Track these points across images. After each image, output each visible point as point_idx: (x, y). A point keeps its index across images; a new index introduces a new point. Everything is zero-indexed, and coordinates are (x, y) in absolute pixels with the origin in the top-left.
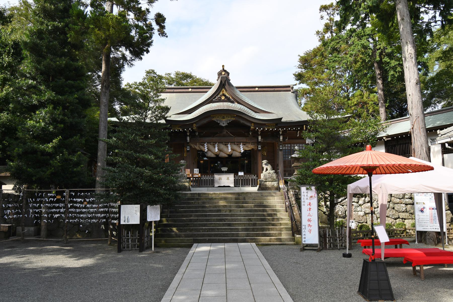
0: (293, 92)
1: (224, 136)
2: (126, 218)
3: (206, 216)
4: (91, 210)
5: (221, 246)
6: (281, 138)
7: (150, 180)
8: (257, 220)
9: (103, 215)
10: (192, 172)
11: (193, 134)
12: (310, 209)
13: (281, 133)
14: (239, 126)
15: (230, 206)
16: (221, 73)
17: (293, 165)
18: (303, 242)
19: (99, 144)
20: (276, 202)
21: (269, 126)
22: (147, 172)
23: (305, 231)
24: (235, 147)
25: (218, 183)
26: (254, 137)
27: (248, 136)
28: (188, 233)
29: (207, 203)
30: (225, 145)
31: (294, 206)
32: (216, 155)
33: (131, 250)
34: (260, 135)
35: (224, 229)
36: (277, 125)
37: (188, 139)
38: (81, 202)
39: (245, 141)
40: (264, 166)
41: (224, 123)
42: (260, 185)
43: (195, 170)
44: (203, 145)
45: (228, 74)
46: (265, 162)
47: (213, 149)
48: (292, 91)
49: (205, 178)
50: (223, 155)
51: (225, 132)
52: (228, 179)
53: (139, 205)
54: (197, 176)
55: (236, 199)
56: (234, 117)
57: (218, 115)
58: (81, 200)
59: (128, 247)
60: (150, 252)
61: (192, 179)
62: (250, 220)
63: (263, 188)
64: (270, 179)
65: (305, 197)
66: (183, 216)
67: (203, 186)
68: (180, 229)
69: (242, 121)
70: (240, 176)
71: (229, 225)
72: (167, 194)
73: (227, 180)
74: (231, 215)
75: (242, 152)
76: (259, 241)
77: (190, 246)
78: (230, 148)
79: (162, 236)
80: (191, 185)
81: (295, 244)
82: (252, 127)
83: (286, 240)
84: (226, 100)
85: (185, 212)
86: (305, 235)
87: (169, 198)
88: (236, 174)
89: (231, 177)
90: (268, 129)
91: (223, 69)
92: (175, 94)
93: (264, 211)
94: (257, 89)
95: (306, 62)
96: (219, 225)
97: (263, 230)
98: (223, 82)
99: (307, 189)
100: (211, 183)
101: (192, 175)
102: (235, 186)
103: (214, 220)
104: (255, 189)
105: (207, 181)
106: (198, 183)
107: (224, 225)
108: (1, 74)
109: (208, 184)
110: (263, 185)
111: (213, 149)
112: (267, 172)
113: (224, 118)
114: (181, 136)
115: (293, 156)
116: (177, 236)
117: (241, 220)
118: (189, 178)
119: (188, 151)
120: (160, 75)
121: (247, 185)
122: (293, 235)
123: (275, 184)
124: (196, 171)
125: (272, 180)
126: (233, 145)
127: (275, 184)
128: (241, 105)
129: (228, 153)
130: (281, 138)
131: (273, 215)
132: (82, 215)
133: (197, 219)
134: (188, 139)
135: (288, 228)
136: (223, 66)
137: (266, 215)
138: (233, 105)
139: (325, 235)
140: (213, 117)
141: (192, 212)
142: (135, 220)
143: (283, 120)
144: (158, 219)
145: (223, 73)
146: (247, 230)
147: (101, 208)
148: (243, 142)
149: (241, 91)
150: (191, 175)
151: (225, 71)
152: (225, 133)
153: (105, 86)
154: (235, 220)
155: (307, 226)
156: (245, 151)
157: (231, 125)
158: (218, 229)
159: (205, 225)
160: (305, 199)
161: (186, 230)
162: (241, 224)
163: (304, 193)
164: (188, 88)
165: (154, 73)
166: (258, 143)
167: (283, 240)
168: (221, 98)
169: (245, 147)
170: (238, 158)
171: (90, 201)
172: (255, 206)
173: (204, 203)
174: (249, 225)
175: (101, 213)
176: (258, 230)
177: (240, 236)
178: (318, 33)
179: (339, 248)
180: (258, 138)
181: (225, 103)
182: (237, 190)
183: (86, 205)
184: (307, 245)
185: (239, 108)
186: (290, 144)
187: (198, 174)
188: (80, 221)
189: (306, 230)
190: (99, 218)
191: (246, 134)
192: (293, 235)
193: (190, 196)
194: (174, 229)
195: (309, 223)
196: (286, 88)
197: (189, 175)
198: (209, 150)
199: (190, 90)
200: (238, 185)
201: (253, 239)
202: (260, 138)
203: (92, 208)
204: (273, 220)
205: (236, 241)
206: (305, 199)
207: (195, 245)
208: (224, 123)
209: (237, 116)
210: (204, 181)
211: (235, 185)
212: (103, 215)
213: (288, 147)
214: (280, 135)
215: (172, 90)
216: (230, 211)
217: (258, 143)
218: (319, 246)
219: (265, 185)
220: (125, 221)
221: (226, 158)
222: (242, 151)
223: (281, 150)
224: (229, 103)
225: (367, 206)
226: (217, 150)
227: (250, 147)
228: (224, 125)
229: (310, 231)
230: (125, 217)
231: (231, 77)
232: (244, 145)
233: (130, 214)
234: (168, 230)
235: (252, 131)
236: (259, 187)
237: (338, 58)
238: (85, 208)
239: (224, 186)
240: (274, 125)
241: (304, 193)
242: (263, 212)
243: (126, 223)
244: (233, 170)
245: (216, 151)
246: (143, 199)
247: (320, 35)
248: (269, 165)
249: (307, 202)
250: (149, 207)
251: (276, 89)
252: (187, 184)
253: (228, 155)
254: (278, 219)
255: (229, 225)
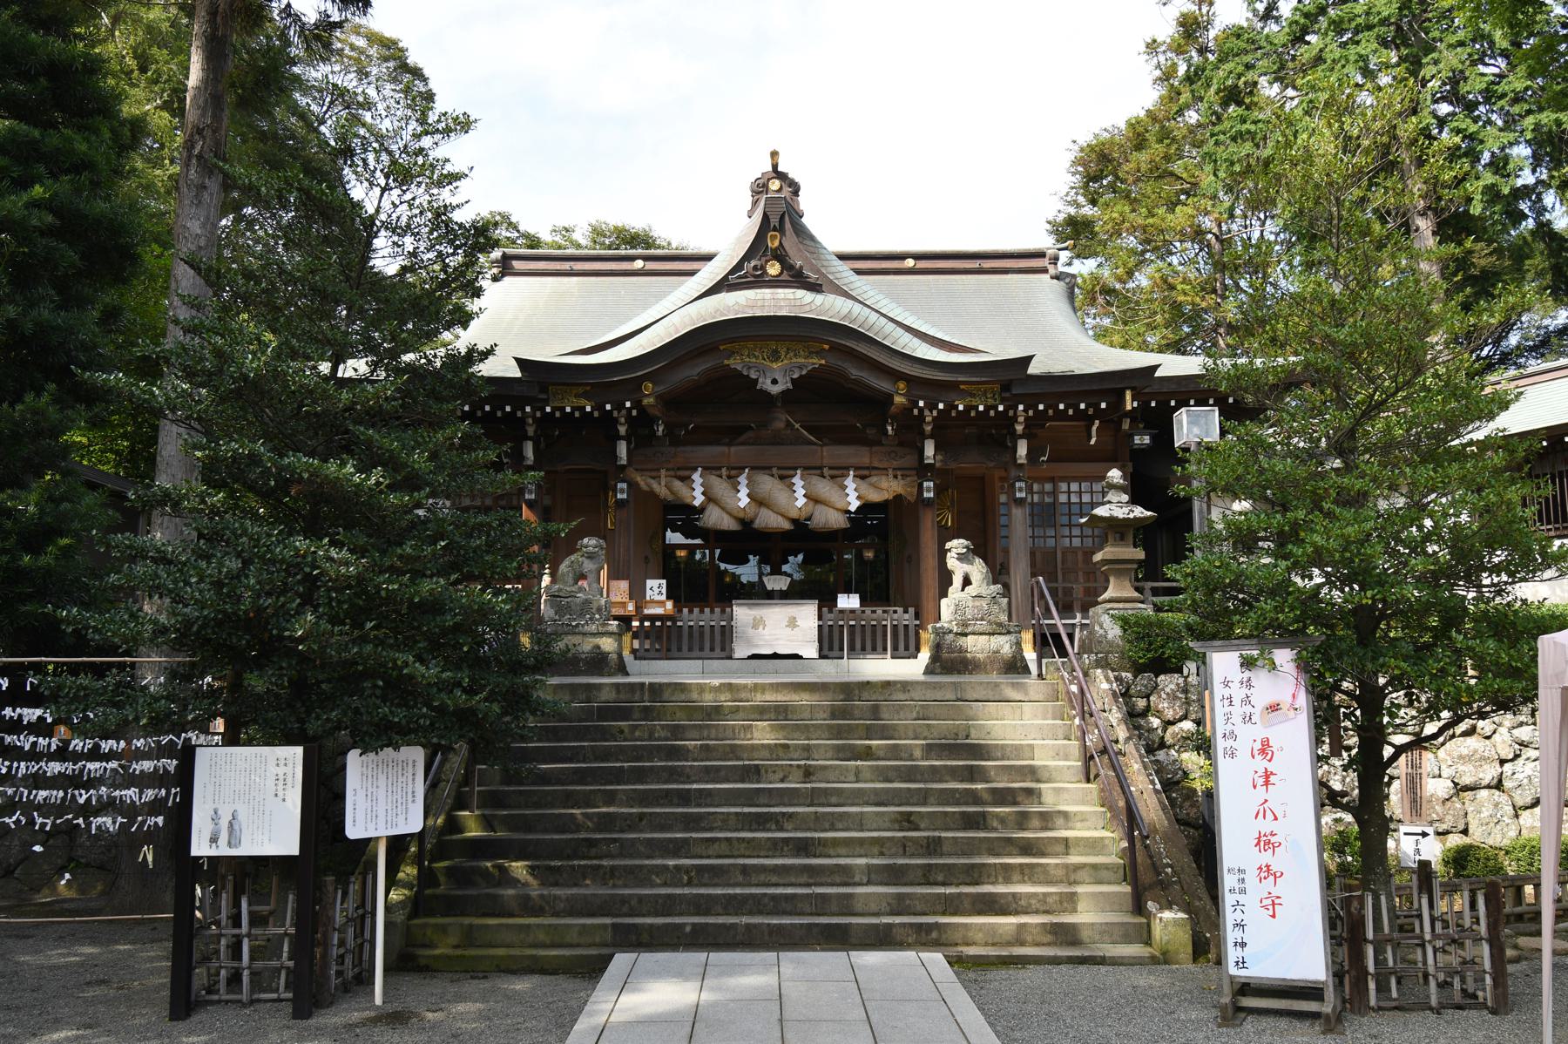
0: (1057, 277)
1: (777, 440)
2: (224, 824)
3: (685, 798)
4: (92, 766)
5: (751, 977)
6: (1022, 450)
7: (360, 604)
8: (946, 822)
9: (150, 794)
10: (637, 593)
11: (641, 425)
12: (1267, 775)
13: (1019, 428)
15: (807, 748)
16: (765, 186)
17: (1098, 557)
18: (1233, 971)
19: (163, 438)
20: (1030, 726)
21: (973, 395)
22: (337, 559)
23: (1242, 905)
24: (824, 488)
25: (749, 642)
26: (901, 444)
27: (879, 443)
28: (590, 889)
29: (695, 734)
30: (782, 478)
31: (1120, 753)
32: (742, 521)
33: (252, 1002)
34: (931, 437)
35: (776, 869)
36: (1006, 387)
37: (622, 449)
38: (40, 728)
39: (866, 461)
40: (952, 562)
41: (775, 377)
42: (937, 648)
43: (650, 583)
44: (686, 480)
45: (795, 188)
46: (957, 545)
47: (732, 498)
48: (1052, 271)
49: (694, 618)
50: (770, 520)
51: (780, 420)
52: (792, 623)
53: (299, 750)
54: (659, 611)
55: (835, 713)
56: (820, 353)
57: (750, 345)
58: (39, 712)
59: (235, 979)
60: (356, 1016)
61: (636, 624)
62: (908, 821)
63: (948, 662)
64: (982, 626)
65: (1238, 711)
66: (570, 800)
67: (696, 653)
68: (550, 868)
69: (855, 372)
70: (842, 611)
71: (803, 847)
72: (459, 684)
73: (783, 628)
74: (814, 797)
75: (853, 508)
76: (957, 937)
77: (593, 969)
78: (800, 492)
79: (452, 906)
80: (634, 651)
81: (1154, 960)
82: (898, 399)
83: (1107, 931)
84: (785, 277)
85: (582, 776)
86: (1240, 925)
87: (473, 712)
88: (826, 601)
89: (807, 615)
90: (968, 409)
91: (775, 167)
93: (972, 774)
94: (910, 263)
95: (1099, 166)
96: (753, 847)
97: (975, 875)
98: (774, 221)
99: (1248, 663)
100: (720, 643)
101: (638, 608)
102: (822, 657)
103: (726, 823)
104: (913, 668)
105: (702, 634)
106: (664, 639)
107: (776, 847)
109: (707, 645)
110: (951, 650)
111: (732, 498)
112: (966, 592)
113: (775, 356)
114: (576, 427)
115: (1101, 511)
116: (528, 907)
117: (860, 823)
118: (625, 620)
119: (621, 504)
120: (532, 231)
121: (874, 649)
122: (1139, 908)
123: (1004, 645)
124: (656, 588)
125: (988, 628)
126: (815, 480)
127: (1004, 645)
128: (850, 303)
129: (794, 514)
130: (1022, 450)
131: (1020, 793)
132: (43, 794)
133: (641, 816)
134: (622, 449)
135: (1106, 867)
136: (774, 154)
137: (986, 796)
138: (819, 299)
139: (1357, 925)
140: (731, 354)
141: (618, 776)
142: (276, 832)
143: (1033, 369)
144: (413, 822)
145: (775, 185)
146: (894, 875)
147: (140, 755)
148: (856, 469)
150: (631, 607)
151: (782, 176)
152: (779, 425)
153: (200, 157)
154: (833, 822)
155: (1251, 877)
156: (866, 507)
157: (806, 390)
158: (745, 869)
159: (678, 848)
160: (1237, 719)
161: (577, 877)
162: (861, 841)
163: (1226, 684)
164: (632, 259)
165: (510, 224)
166: (923, 470)
167: (1085, 935)
168: (763, 268)
169: (864, 485)
170: (832, 535)
171: (86, 719)
172: (929, 750)
173: (677, 732)
174: (904, 847)
175: (142, 781)
176: (951, 875)
177: (859, 907)
178: (1152, 47)
179: (1434, 1002)
180: (921, 451)
182: (831, 671)
183: (66, 743)
184: (1246, 988)
185: (845, 311)
186: (1052, 480)
187: (662, 603)
188: (32, 822)
189: (1251, 900)
190: (131, 811)
191: (871, 432)
192: (1139, 908)
193: (613, 695)
194: (519, 868)
195: (1266, 858)
196: (1026, 261)
197: (624, 605)
198: (710, 498)
199: (639, 264)
200: (836, 653)
201: (929, 928)
202: (929, 450)
203: (95, 754)
204: (1022, 820)
205: (839, 939)
206: (1237, 719)
207: (621, 961)
208: (775, 377)
209: (835, 348)
210: (691, 635)
211: (821, 649)
212: (150, 794)
213: (1042, 493)
214: (1015, 437)
215: (566, 266)
216: (808, 773)
217: (923, 470)
218: (1330, 994)
219: (962, 650)
220: (214, 840)
221: (784, 534)
222: (854, 505)
223: (1020, 502)
224: (800, 293)
225: (1465, 752)
226: (744, 500)
227: (886, 488)
228: (775, 390)
229: (1272, 905)
230: (216, 816)
231: (804, 202)
232: (863, 478)
233: (248, 800)
234: (485, 874)
235: (894, 418)
236: (935, 658)
237: (1255, 122)
238: (62, 754)
239: (775, 656)
240: (997, 387)
241: (1226, 684)
242: (972, 780)
243: (223, 850)
244: (818, 590)
245: (742, 504)
246: (322, 720)
247: (1162, 58)
248: (978, 561)
249: (1248, 737)
250: (354, 759)
251: (988, 264)
252: (608, 644)
253: (794, 521)
254: (1047, 819)
255: (803, 847)
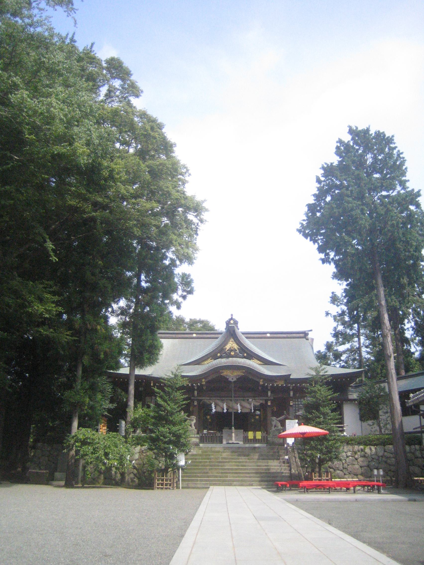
14: (250, 383)
92: (177, 340)
108: (4, 330)
136: (232, 315)
143: (291, 377)
149: (247, 338)
157: (241, 380)
181: (235, 359)
199: (194, 335)
